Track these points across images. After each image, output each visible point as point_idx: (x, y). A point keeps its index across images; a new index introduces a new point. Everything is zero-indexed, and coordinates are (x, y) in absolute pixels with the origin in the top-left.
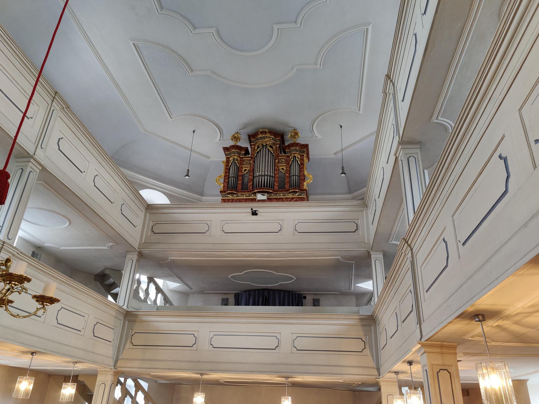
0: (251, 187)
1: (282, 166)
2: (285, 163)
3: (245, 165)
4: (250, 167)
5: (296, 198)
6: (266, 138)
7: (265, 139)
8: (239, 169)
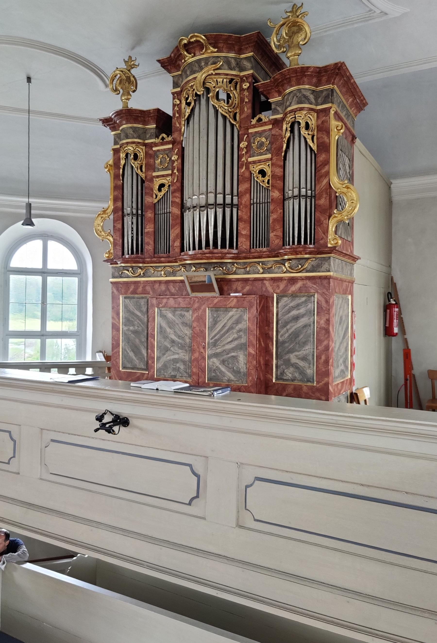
0: (178, 243)
1: (260, 161)
2: (268, 151)
3: (159, 170)
4: (171, 175)
5: (302, 279)
6: (207, 64)
7: (201, 68)
8: (146, 184)
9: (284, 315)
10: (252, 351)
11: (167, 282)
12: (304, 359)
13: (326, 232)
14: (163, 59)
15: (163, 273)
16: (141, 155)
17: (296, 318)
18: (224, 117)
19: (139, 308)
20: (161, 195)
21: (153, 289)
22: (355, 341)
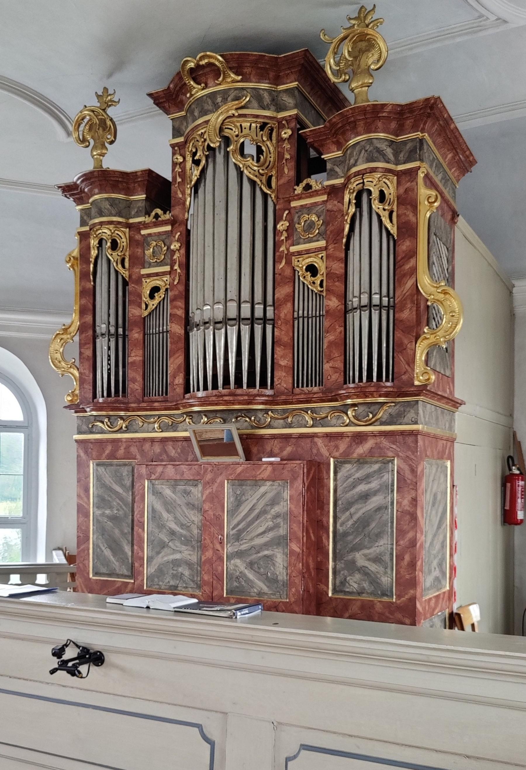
0: (180, 380)
3: (150, 266)
4: (170, 273)
5: (374, 435)
6: (225, 100)
7: (217, 107)
9: (345, 492)
10: (296, 547)
11: (164, 440)
12: (377, 560)
13: (411, 362)
14: (157, 93)
15: (156, 425)
16: (123, 242)
17: (365, 497)
18: (253, 183)
19: (119, 480)
20: (153, 305)
21: (142, 452)
22: (456, 533)
